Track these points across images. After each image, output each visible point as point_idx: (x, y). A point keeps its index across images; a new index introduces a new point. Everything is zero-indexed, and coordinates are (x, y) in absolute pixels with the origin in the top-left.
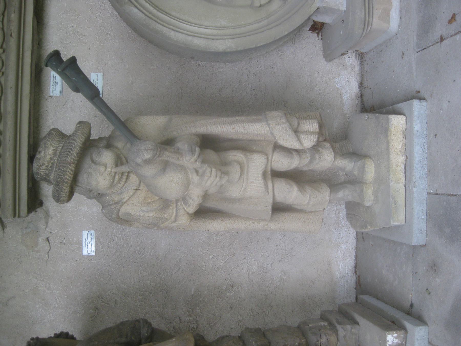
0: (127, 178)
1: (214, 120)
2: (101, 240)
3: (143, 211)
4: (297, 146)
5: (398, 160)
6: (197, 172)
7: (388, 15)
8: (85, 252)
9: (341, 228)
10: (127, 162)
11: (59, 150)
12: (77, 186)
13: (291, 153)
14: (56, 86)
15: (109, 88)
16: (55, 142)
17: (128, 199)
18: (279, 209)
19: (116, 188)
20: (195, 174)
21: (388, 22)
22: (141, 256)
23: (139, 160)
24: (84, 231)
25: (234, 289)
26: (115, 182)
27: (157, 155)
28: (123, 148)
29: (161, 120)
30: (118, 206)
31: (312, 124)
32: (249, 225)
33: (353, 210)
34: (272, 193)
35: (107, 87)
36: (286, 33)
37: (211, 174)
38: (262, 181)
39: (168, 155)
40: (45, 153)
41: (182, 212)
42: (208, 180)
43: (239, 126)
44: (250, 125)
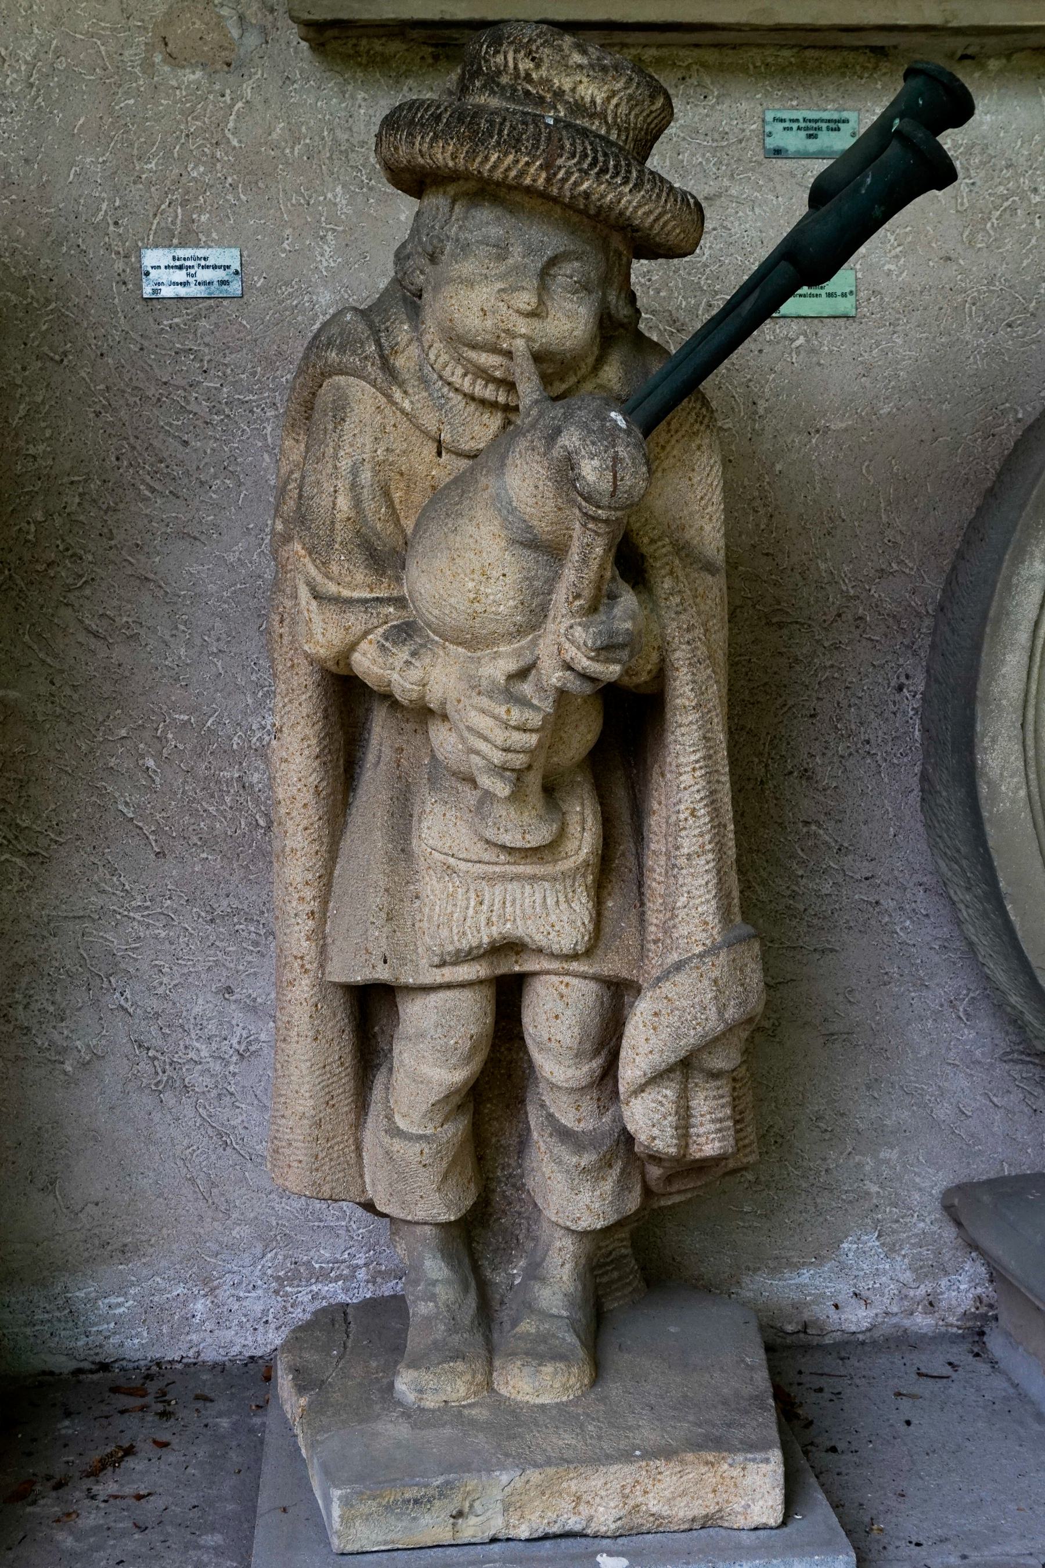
0: (483, 402)
1: (721, 736)
2: (203, 322)
3: (355, 472)
4: (633, 1067)
6: (522, 674)
8: (152, 257)
9: (276, 1292)
10: (555, 399)
11: (595, 126)
12: (453, 203)
13: (596, 1053)
14: (803, 134)
15: (797, 343)
16: (623, 110)
17: (402, 411)
19: (444, 357)
20: (512, 666)
22: (143, 481)
23: (570, 439)
24: (236, 252)
25: (19, 861)
26: (472, 355)
27: (591, 510)
28: (600, 386)
29: (709, 532)
30: (372, 370)
31: (720, 1130)
32: (301, 899)
33: (363, 1334)
34: (439, 980)
35: (806, 335)
37: (517, 728)
38: (486, 940)
39: (587, 553)
40: (580, 67)
41: (357, 621)
42: (496, 718)
43: (701, 834)
44: (707, 877)
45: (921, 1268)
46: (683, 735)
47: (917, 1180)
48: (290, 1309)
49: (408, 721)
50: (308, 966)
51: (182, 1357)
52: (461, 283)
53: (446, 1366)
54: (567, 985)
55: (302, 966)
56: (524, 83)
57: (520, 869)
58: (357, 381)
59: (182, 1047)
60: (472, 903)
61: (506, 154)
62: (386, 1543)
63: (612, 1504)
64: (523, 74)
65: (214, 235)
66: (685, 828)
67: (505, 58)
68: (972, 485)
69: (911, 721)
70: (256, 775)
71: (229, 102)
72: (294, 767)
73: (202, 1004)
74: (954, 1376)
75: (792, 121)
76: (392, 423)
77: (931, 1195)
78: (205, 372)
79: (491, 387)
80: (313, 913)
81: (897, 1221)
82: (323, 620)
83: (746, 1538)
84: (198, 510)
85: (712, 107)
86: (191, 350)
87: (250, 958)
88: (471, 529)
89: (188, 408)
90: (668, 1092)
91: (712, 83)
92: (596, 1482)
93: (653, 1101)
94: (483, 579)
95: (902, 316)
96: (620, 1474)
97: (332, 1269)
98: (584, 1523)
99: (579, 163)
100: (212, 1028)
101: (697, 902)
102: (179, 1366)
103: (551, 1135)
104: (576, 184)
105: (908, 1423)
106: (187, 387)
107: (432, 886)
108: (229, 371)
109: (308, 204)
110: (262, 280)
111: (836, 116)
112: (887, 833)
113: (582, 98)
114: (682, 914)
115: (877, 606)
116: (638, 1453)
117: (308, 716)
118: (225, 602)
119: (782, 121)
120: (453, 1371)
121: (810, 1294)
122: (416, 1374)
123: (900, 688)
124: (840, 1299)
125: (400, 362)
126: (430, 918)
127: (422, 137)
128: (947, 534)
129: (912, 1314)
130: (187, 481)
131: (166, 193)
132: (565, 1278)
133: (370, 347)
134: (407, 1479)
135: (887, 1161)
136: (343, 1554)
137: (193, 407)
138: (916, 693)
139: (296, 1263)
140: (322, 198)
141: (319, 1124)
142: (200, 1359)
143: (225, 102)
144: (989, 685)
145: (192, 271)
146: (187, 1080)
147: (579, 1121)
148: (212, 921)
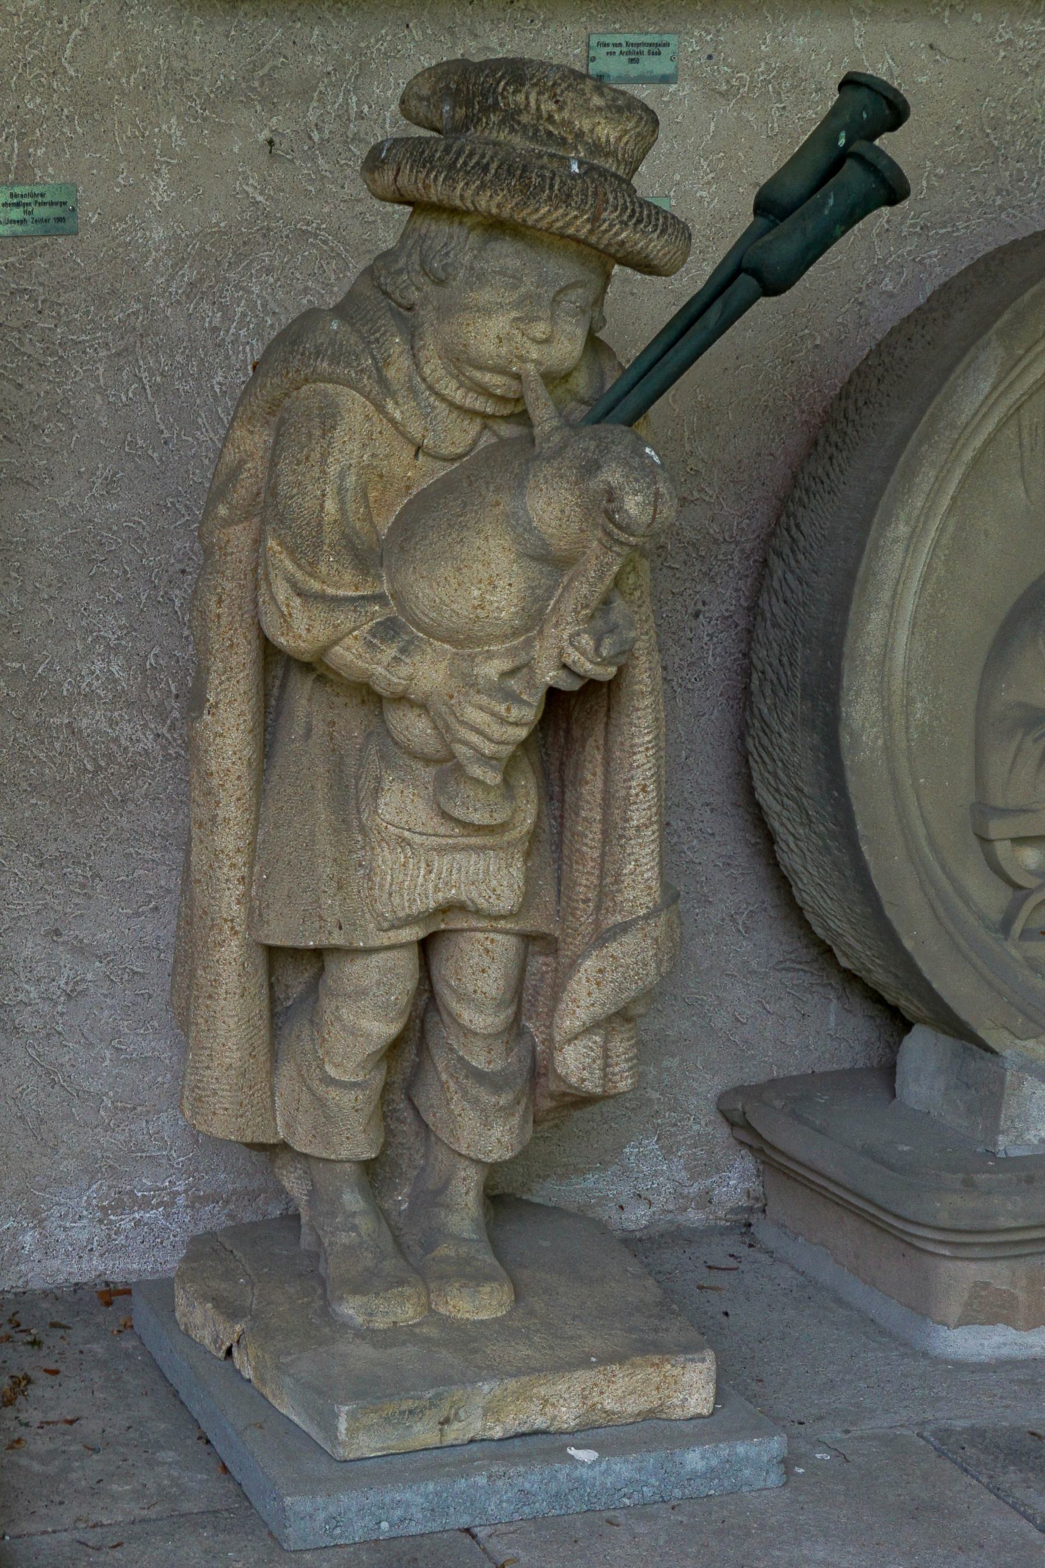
3: (342, 476)
5: (561, 1402)
7: (992, 1320)
9: (100, 1221)
14: (625, 59)
17: (392, 421)
18: (295, 974)
21: (965, 1321)
23: (612, 475)
26: (477, 375)
28: (569, 391)
31: (630, 1068)
32: (233, 866)
34: (386, 943)
36: (908, 944)
40: (600, 109)
41: (344, 619)
42: (493, 714)
43: (650, 808)
44: (652, 847)
45: (695, 1167)
46: (639, 718)
47: (695, 1085)
48: (114, 1236)
49: (338, 695)
50: (238, 928)
51: (12, 1287)
52: (478, 311)
53: (395, 1291)
54: (492, 941)
55: (232, 928)
56: (546, 124)
57: (473, 840)
58: (346, 390)
59: (12, 989)
60: (422, 872)
61: (556, 208)
62: (383, 1449)
63: (573, 1405)
64: (545, 115)
65: (50, 170)
66: (635, 803)
67: (527, 98)
68: (770, 411)
69: (706, 647)
70: (85, 721)
71: (66, 29)
72: (229, 741)
73: (30, 948)
74: (742, 1267)
75: (615, 45)
76: (379, 429)
77: (707, 1099)
78: (40, 312)
79: (481, 399)
80: (243, 878)
81: (675, 1125)
82: (310, 617)
83: (688, 1428)
84: (31, 454)
85: (538, 31)
86: (26, 289)
87: (77, 901)
88: (479, 542)
89: (22, 349)
90: (597, 1039)
91: (539, 7)
92: (561, 1387)
93: (585, 1048)
94: (490, 588)
95: (711, 244)
96: (582, 1378)
97: (154, 1196)
98: (549, 1422)
99: (621, 215)
100: (41, 969)
101: (644, 869)
102: (10, 1296)
103: (467, 1077)
104: (616, 234)
105: (726, 1314)
106: (22, 328)
107: (386, 859)
108: (63, 311)
109: (143, 137)
110: (97, 216)
111: (656, 39)
112: (679, 756)
113: (599, 139)
114: (628, 881)
115: (678, 534)
116: (593, 1359)
117: (245, 693)
118: (56, 548)
119: (606, 45)
120: (401, 1295)
121: (594, 1197)
122: (365, 1299)
123: (697, 615)
124: (623, 1199)
125: (391, 373)
126: (382, 886)
127: (467, 184)
128: (746, 461)
129: (685, 1211)
130: (20, 425)
131: (3, 126)
132: (470, 1205)
133: (367, 360)
134: (403, 1393)
135: (668, 1069)
136: (345, 1461)
137: (27, 349)
138: (711, 620)
139: (120, 1193)
140: (157, 130)
141: (243, 1075)
142: (28, 1288)
143: (62, 29)
144: (855, 642)
145: (30, 209)
146: (17, 1022)
147: (489, 1063)
148: (41, 865)
